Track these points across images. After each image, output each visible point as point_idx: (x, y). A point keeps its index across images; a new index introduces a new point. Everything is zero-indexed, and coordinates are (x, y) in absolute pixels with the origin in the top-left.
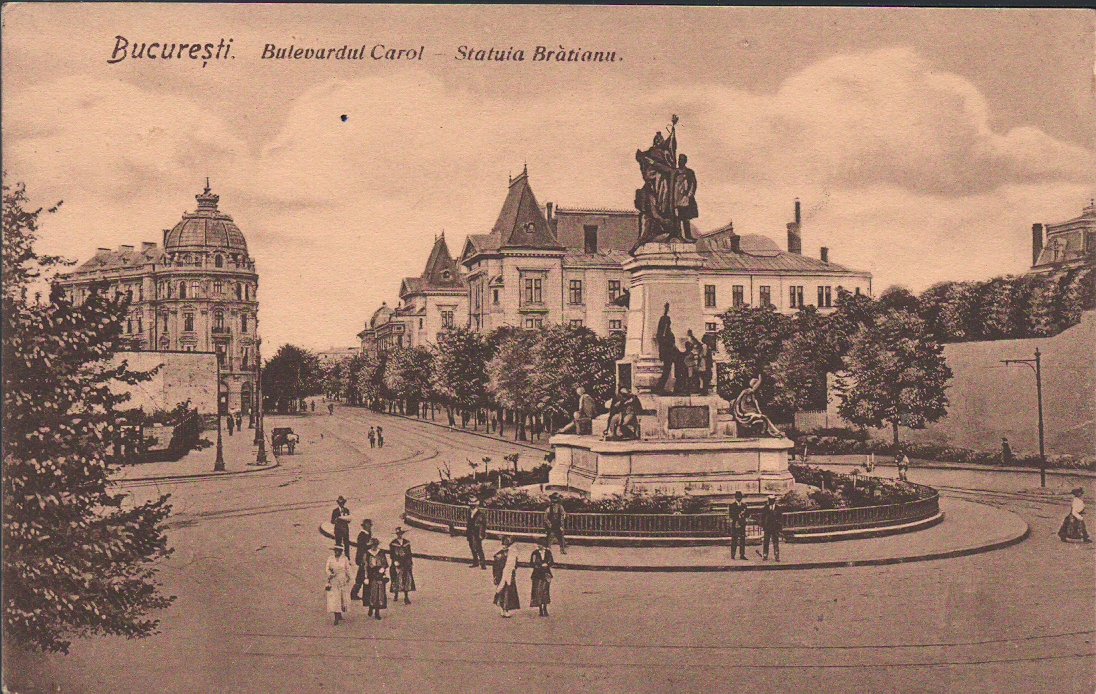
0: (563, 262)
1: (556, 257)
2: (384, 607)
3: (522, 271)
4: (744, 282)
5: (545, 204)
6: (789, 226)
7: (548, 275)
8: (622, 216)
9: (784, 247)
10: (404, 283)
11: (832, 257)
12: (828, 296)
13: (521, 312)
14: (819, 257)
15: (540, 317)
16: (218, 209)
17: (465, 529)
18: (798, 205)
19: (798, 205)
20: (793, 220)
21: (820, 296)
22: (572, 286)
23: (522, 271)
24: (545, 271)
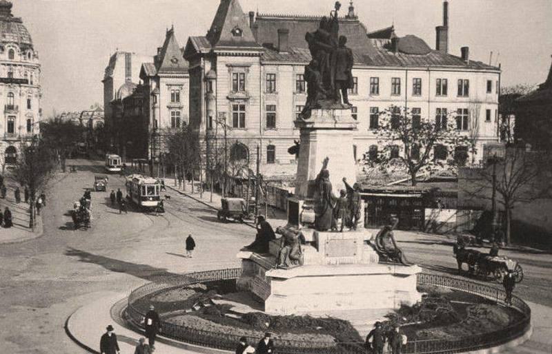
0: (261, 59)
1: (256, 55)
2: (297, 81)
3: (230, 66)
4: (400, 74)
5: (248, 13)
6: (438, 29)
7: (250, 68)
8: (308, 21)
9: (433, 47)
10: (142, 67)
11: (472, 57)
12: (445, 119)
13: (228, 98)
14: (459, 55)
15: (243, 103)
16: (12, 13)
17: (144, 331)
18: (446, 4)
19: (446, 4)
20: (441, 24)
21: (438, 118)
22: (268, 79)
23: (230, 66)
24: (247, 66)
